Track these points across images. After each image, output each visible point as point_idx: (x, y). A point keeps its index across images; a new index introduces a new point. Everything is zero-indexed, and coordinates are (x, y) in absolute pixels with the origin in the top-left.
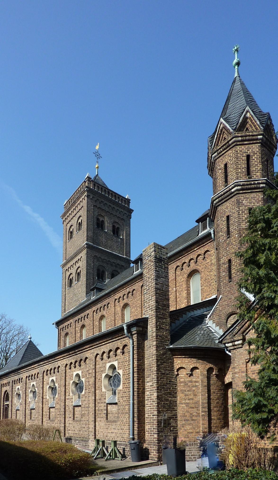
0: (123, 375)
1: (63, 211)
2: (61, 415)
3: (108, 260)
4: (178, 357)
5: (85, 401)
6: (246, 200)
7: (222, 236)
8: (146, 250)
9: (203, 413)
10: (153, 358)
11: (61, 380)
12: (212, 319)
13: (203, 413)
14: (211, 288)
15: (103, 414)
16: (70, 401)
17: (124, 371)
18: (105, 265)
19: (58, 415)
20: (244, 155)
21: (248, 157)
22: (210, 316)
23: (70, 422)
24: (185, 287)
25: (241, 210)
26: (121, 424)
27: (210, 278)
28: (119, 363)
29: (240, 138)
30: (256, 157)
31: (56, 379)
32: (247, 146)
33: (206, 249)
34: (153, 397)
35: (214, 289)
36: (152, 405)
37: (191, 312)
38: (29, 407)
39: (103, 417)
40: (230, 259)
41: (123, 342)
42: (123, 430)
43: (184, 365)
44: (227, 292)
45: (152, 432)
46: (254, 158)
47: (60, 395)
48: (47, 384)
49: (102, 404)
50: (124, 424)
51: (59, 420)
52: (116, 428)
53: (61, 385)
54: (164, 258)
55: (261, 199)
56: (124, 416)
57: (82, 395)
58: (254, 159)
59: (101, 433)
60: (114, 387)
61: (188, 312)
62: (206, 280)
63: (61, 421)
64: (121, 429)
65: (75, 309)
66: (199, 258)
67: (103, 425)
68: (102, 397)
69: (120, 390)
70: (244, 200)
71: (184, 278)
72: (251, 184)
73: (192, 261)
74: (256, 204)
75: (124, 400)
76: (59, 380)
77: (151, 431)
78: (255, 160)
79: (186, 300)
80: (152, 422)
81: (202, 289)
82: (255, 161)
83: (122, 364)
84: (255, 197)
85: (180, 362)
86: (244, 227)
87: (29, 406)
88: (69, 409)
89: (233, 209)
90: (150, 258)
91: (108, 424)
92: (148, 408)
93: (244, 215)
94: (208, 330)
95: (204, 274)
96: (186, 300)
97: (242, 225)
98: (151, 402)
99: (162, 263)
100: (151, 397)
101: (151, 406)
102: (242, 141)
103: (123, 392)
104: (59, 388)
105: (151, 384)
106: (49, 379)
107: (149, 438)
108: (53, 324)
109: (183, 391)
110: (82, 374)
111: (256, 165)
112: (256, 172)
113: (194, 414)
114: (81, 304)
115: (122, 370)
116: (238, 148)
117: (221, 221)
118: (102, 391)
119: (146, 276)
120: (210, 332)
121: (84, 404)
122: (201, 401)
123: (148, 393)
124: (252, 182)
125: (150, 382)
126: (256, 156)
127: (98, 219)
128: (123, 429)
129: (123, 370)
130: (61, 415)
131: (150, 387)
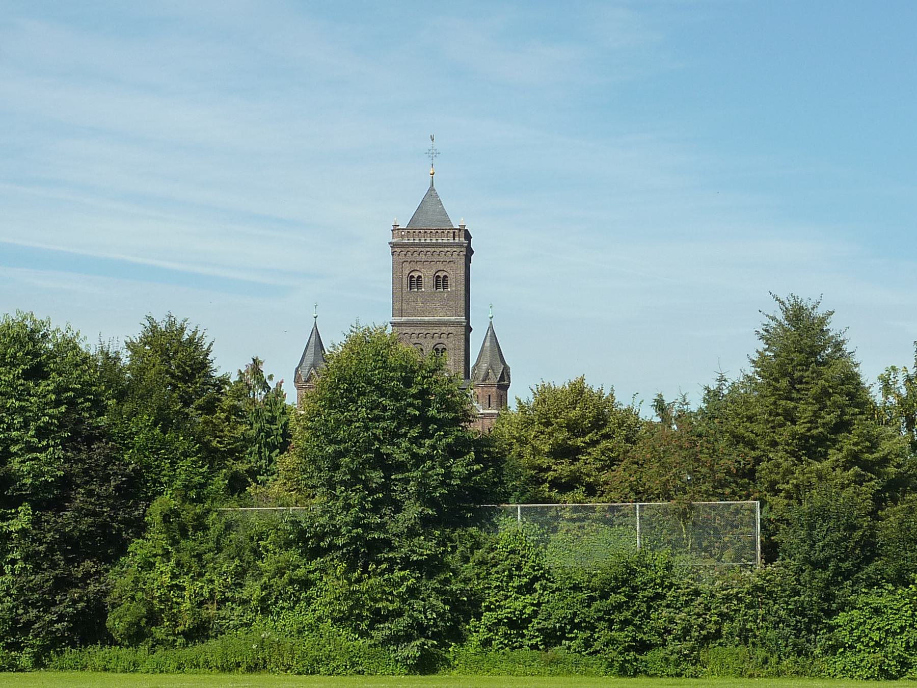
18: (422, 341)
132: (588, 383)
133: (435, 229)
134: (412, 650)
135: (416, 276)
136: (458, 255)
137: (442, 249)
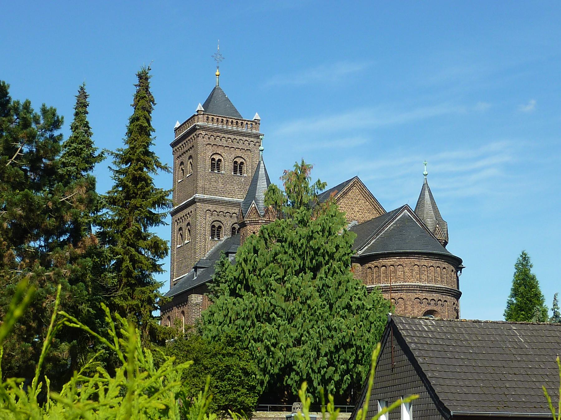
18: (222, 219)
132: (133, 104)
133: (236, 119)
134: (246, 259)
135: (217, 159)
136: (255, 145)
137: (241, 138)
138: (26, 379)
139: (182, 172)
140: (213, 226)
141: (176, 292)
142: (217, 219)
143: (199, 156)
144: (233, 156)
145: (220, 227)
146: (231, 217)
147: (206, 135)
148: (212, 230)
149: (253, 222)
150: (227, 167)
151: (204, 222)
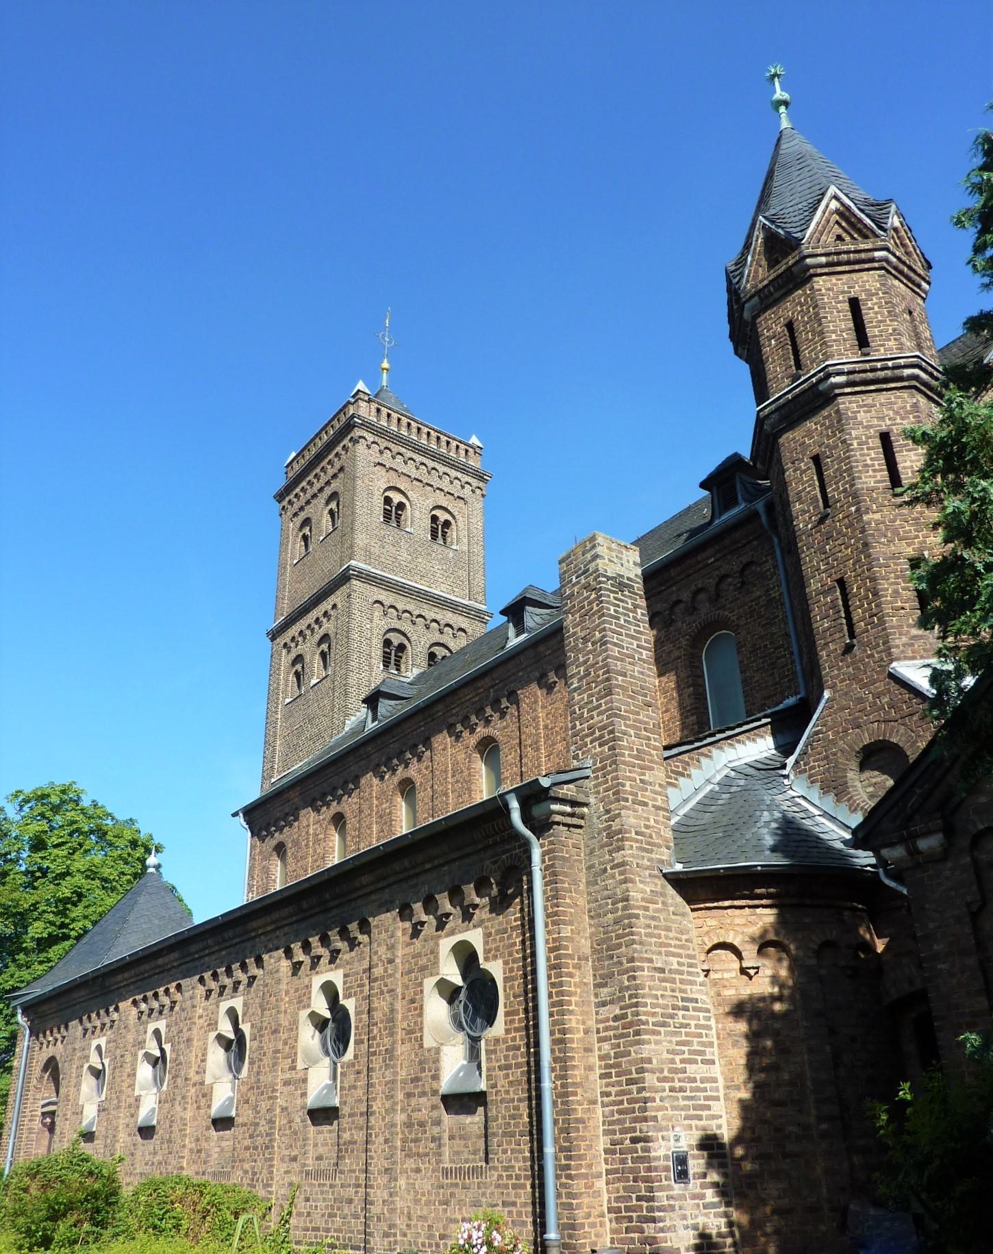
0: (506, 980)
1: (281, 482)
2: (256, 1148)
3: (416, 613)
4: (707, 905)
5: (355, 1087)
6: (864, 412)
7: (804, 512)
8: (568, 556)
9: (824, 1126)
10: (620, 913)
11: (263, 1010)
12: (805, 771)
13: (824, 1126)
14: (776, 675)
15: (426, 1139)
16: (296, 1090)
17: (511, 965)
18: (406, 627)
19: (247, 1148)
20: (841, 298)
21: (855, 304)
22: (797, 762)
23: (294, 1178)
24: (688, 677)
25: (856, 438)
26: (505, 1181)
27: (771, 643)
28: (487, 935)
29: (823, 260)
30: (876, 304)
31: (245, 1005)
32: (845, 277)
33: (744, 560)
34: (630, 1062)
35: (788, 676)
36: (625, 1098)
37: (726, 748)
38: (132, 1120)
39: (427, 1155)
40: (842, 578)
41: (504, 857)
42: (514, 1209)
43: (732, 934)
44: (843, 681)
45: (634, 1215)
46: (870, 305)
47: (259, 1067)
48: (209, 1025)
49: (423, 1100)
50: (514, 1181)
51: (246, 1172)
52: (484, 1200)
53: (261, 1028)
54: (628, 579)
55: (911, 406)
56: (513, 1146)
57: (344, 1063)
58: (873, 309)
59: (420, 1224)
60: (471, 1029)
61: (718, 751)
62: (381, 817)
63: (254, 1174)
64: (504, 1204)
65: (314, 761)
66: (724, 586)
67: (427, 1187)
68: (423, 1070)
69: (497, 1041)
70: (859, 412)
71: (680, 648)
72: (873, 370)
73: (702, 596)
74: (898, 421)
75: (511, 1078)
76: (255, 1009)
77: (628, 1209)
78: (876, 308)
79: (695, 717)
80: (632, 1171)
81: (744, 681)
82: (876, 313)
83: (502, 939)
84: (891, 403)
85: (713, 923)
86: (872, 484)
87: (132, 1116)
88: (290, 1122)
89: (829, 437)
90: (586, 578)
91: (449, 1181)
92: (611, 1108)
93: (866, 451)
94: (795, 809)
95: (748, 633)
96: (695, 717)
97: (864, 479)
98: (619, 1083)
99: (626, 593)
100: (618, 1065)
101: (621, 1102)
102: (828, 265)
103: (508, 1049)
104: (255, 1039)
105: (618, 1012)
106: (218, 1007)
107: (622, 1239)
108: (235, 815)
109: (735, 1035)
110: (345, 983)
111: (881, 321)
112: (884, 340)
113: (791, 1128)
114: (332, 749)
115: (500, 961)
116: (821, 283)
117: (794, 471)
118: (421, 1046)
119: (575, 633)
120: (802, 815)
121: (349, 1100)
122: (808, 1075)
123: (607, 1047)
124: (879, 365)
125: (612, 1002)
126: (875, 300)
127: (388, 501)
128: (514, 1204)
129: (506, 963)
130: (256, 1148)
131: (611, 1023)
136: (473, 491)
138: (773, 1011)
139: (303, 543)
140: (387, 643)
141: (320, 759)
142: (397, 627)
143: (359, 482)
144: (430, 503)
145: (402, 648)
146: (428, 627)
147: (373, 443)
148: (384, 652)
149: (844, 257)
150: (417, 520)
151: (368, 626)
